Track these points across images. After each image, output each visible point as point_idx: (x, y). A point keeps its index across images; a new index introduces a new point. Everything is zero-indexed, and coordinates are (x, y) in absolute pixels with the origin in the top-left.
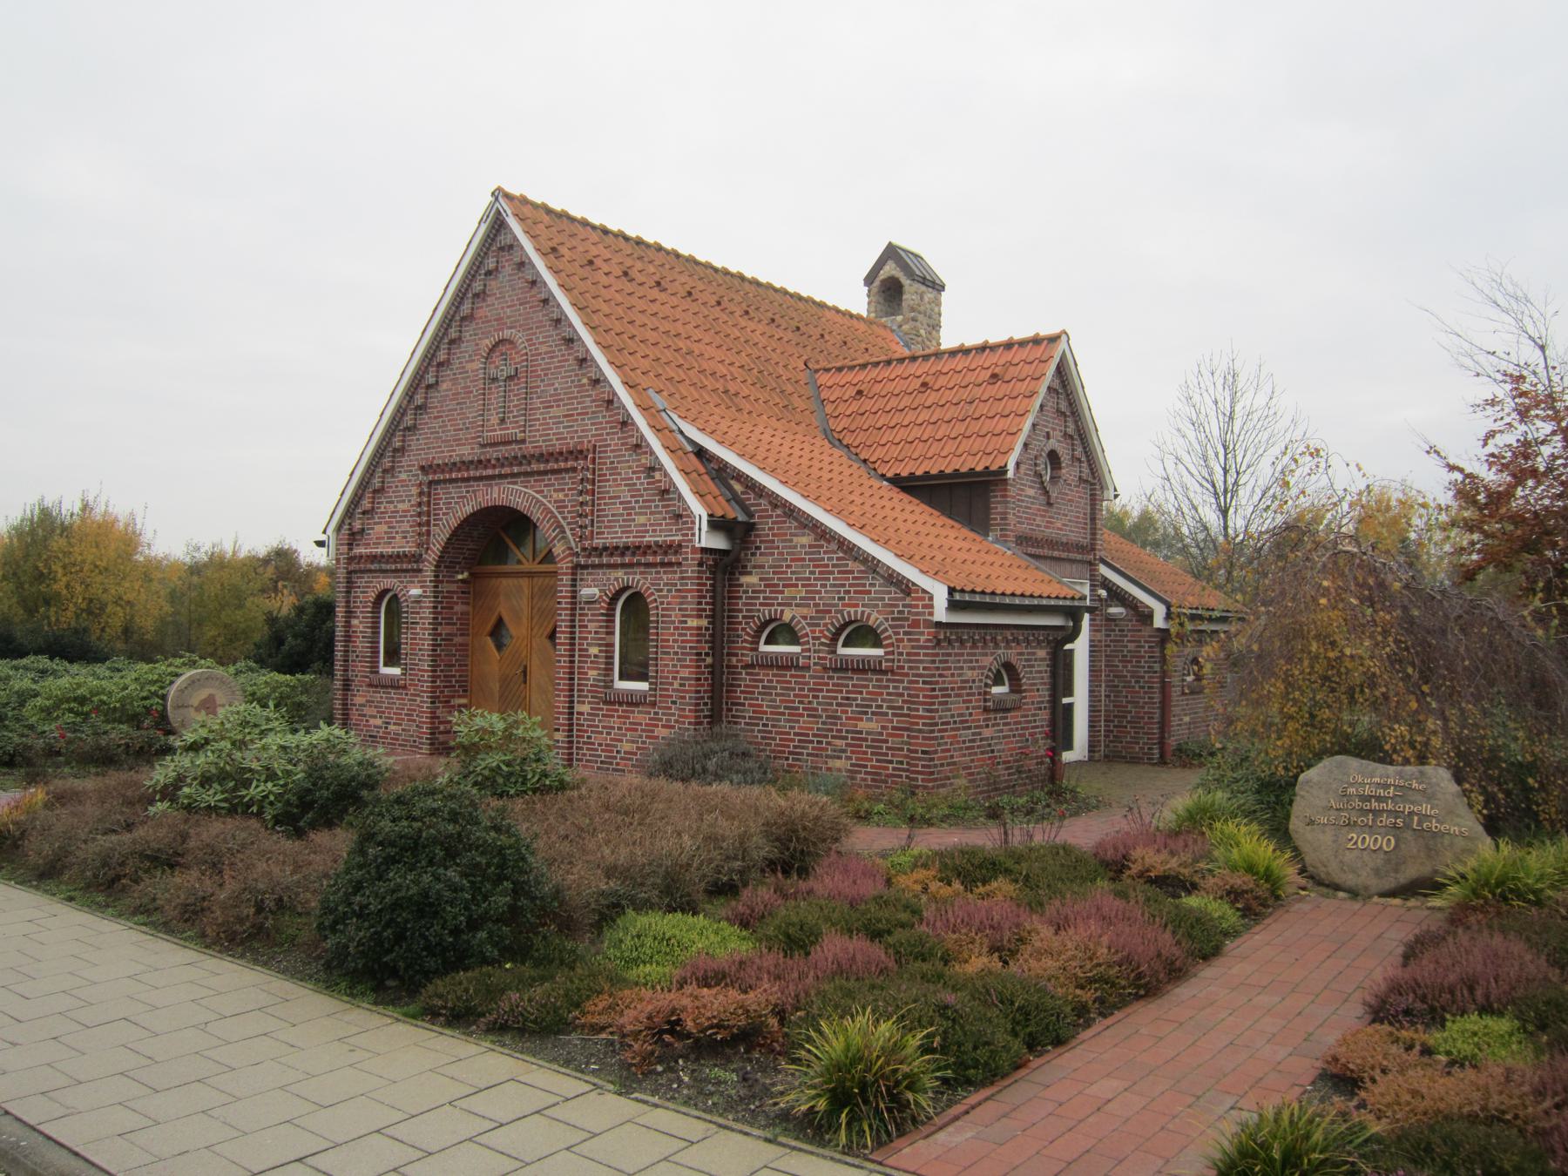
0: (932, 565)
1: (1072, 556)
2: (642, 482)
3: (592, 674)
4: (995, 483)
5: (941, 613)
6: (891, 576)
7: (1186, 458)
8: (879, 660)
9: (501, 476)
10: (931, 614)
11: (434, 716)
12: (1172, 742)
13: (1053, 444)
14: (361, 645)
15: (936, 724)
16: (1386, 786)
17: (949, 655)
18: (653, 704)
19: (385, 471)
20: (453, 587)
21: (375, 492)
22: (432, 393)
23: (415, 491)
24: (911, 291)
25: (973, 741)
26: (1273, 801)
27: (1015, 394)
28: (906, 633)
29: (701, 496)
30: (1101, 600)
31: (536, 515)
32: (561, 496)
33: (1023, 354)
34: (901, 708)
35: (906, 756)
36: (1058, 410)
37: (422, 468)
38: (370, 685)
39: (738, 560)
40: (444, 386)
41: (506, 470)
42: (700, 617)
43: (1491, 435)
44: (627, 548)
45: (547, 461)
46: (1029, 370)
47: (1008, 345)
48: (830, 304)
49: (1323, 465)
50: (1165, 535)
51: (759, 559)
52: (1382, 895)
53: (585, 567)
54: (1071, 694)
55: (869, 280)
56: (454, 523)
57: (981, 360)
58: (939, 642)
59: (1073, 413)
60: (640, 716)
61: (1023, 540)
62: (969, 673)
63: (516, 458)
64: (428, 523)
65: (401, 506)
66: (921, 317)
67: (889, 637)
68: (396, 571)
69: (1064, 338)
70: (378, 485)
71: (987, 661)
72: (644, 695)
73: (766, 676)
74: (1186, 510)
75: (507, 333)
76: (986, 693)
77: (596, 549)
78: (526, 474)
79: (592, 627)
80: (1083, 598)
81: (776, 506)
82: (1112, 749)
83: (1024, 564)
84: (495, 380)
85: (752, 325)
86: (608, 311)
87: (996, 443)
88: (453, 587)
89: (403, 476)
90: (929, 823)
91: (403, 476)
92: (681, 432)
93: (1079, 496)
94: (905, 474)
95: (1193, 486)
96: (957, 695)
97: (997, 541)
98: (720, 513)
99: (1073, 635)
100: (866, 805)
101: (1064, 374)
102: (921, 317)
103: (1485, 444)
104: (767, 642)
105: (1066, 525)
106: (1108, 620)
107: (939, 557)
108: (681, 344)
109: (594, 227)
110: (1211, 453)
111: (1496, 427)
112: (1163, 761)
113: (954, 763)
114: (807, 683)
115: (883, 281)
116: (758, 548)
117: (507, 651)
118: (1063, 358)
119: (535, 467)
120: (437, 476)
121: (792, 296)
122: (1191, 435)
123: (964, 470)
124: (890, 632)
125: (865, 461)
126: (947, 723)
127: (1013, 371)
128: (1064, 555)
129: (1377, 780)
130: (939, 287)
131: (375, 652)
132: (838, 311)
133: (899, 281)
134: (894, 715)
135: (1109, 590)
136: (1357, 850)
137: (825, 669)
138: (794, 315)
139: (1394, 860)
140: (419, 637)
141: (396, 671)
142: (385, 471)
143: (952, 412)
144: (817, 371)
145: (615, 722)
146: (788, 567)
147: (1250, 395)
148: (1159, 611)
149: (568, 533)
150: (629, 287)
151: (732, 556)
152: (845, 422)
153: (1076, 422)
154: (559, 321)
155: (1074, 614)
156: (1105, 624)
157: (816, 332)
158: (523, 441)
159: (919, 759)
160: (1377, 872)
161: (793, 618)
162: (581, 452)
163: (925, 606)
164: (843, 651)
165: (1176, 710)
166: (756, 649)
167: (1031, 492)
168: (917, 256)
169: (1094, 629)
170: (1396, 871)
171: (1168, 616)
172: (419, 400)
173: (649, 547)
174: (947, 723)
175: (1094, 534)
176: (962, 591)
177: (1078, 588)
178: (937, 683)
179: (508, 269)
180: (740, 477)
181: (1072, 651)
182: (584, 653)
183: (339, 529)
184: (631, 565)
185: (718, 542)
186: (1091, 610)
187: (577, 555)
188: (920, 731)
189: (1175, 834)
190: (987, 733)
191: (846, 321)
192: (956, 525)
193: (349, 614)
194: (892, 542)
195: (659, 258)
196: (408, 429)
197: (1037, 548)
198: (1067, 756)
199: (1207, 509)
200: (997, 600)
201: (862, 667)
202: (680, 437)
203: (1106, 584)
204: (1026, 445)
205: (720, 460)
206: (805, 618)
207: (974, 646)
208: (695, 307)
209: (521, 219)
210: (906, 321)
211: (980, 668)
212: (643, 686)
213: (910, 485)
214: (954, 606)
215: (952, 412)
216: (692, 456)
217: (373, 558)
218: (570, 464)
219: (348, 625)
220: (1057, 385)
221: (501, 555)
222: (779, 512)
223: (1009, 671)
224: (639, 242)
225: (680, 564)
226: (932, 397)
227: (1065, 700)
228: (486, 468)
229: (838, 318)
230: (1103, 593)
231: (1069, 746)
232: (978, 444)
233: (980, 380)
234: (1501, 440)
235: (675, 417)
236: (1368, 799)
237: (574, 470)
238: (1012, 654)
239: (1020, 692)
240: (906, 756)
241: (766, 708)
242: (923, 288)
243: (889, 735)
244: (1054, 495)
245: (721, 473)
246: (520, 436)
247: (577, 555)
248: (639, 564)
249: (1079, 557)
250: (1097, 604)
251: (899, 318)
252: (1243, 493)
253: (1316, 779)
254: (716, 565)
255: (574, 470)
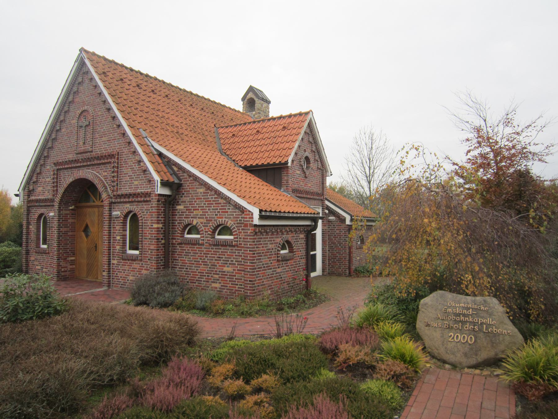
0: (252, 200)
1: (315, 197)
2: (136, 167)
3: (118, 247)
4: (284, 168)
5: (256, 221)
6: (236, 205)
7: (356, 163)
8: (231, 241)
9: (84, 166)
10: (252, 221)
11: (59, 265)
12: (353, 268)
13: (307, 154)
14: (33, 236)
15: (256, 269)
16: (468, 309)
17: (261, 238)
18: (141, 260)
19: (41, 165)
20: (68, 212)
21: (38, 174)
22: (59, 133)
23: (52, 173)
24: (258, 103)
25: (273, 274)
26: (407, 310)
27: (292, 134)
28: (242, 229)
29: (158, 172)
30: (326, 214)
31: (96, 182)
32: (106, 174)
33: (295, 119)
34: (241, 262)
35: (243, 282)
36: (309, 141)
37: (54, 164)
38: (36, 253)
39: (175, 199)
40: (63, 130)
41: (85, 164)
42: (158, 223)
43: (469, 151)
44: (130, 195)
45: (100, 159)
46: (297, 125)
47: (290, 116)
48: (227, 106)
49: (421, 153)
50: (347, 194)
51: (184, 199)
52: (469, 367)
53: (115, 203)
54: (315, 250)
55: (243, 99)
56: (66, 186)
57: (279, 122)
58: (256, 233)
59: (315, 143)
60: (136, 265)
61: (295, 191)
62: (271, 246)
63: (89, 158)
64: (57, 186)
65: (47, 180)
66: (262, 112)
67: (236, 231)
68: (45, 206)
69: (311, 113)
70: (38, 171)
71: (279, 240)
72: (137, 256)
73: (187, 248)
74: (356, 182)
75: (86, 108)
76: (278, 254)
77: (119, 195)
78: (93, 165)
79: (118, 228)
80: (318, 213)
81: (190, 176)
82: (331, 271)
83: (295, 200)
84: (81, 127)
85: (193, 110)
86: (126, 98)
87: (284, 152)
88: (68, 212)
89: (48, 167)
90: (250, 315)
91: (48, 167)
92: (153, 146)
93: (317, 174)
94: (248, 165)
95: (359, 174)
96: (265, 256)
97: (284, 191)
98: (166, 179)
99: (315, 228)
100: (222, 307)
101: (310, 126)
102: (262, 112)
103: (467, 155)
104: (188, 233)
105: (312, 186)
106: (329, 221)
107: (258, 196)
108: (159, 113)
109: (126, 68)
110: (364, 162)
111: (470, 148)
112: (350, 275)
113: (264, 285)
114: (203, 251)
115: (248, 100)
116: (183, 194)
117: (90, 237)
118: (311, 120)
119: (96, 162)
120: (61, 167)
121: (212, 102)
122: (358, 155)
123: (271, 163)
124: (236, 229)
125: (234, 160)
126: (261, 268)
127: (292, 126)
128: (312, 197)
129: (462, 305)
130: (268, 102)
131: (38, 239)
132: (230, 109)
133: (254, 99)
134: (238, 264)
135: (329, 210)
136: (455, 343)
137: (210, 245)
138: (212, 108)
139: (474, 349)
140: (53, 233)
141: (45, 246)
142: (41, 165)
143: (268, 141)
144: (219, 128)
145: (126, 268)
146: (195, 202)
147: (378, 141)
148: (348, 218)
149: (109, 189)
150: (139, 91)
151: (172, 197)
152: (227, 146)
153: (316, 146)
154: (105, 102)
155: (315, 220)
156: (327, 223)
157: (220, 115)
158: (92, 152)
159: (248, 284)
160: (465, 354)
161: (197, 223)
162: (113, 155)
163: (250, 218)
164: (218, 237)
165: (354, 255)
166: (183, 237)
167: (298, 172)
168: (260, 91)
169: (323, 225)
170: (476, 355)
171: (352, 220)
172: (53, 136)
173: (139, 194)
174: (261, 268)
175: (323, 189)
176: (266, 211)
177: (317, 210)
178: (256, 251)
179: (87, 81)
180: (176, 164)
181: (315, 234)
182: (115, 240)
183: (24, 189)
184: (132, 202)
185: (166, 191)
186: (321, 218)
187: (111, 198)
188: (248, 272)
189: (360, 328)
190: (279, 270)
191: (233, 112)
192: (268, 185)
193: (28, 224)
194: (237, 191)
195: (155, 82)
196: (49, 148)
197: (301, 194)
198: (313, 275)
199: (364, 181)
200: (282, 215)
201: (225, 244)
202: (152, 148)
203: (328, 208)
204: (296, 154)
205: (168, 158)
206: (202, 223)
207: (273, 234)
208: (168, 101)
209: (91, 61)
210: (256, 114)
211: (275, 243)
212: (137, 252)
213: (252, 170)
214: (262, 217)
215: (268, 141)
216: (157, 157)
217: (37, 201)
218: (109, 160)
219: (28, 228)
220: (308, 131)
221: (87, 199)
222: (191, 179)
223: (288, 244)
224: (147, 76)
225: (150, 201)
226: (261, 136)
227: (312, 253)
228: (77, 163)
229: (231, 111)
230: (327, 211)
231: (314, 270)
232: (278, 153)
233: (279, 129)
234: (472, 153)
235: (150, 140)
236: (458, 315)
237: (110, 163)
238: (289, 237)
239: (293, 252)
240: (243, 282)
241: (187, 262)
242: (263, 102)
243: (236, 273)
244: (307, 174)
245: (169, 163)
246: (90, 149)
247: (111, 198)
248: (135, 201)
249: (318, 198)
250: (324, 216)
251: (254, 113)
252: (376, 176)
253: (430, 303)
254: (166, 201)
255: (110, 163)
